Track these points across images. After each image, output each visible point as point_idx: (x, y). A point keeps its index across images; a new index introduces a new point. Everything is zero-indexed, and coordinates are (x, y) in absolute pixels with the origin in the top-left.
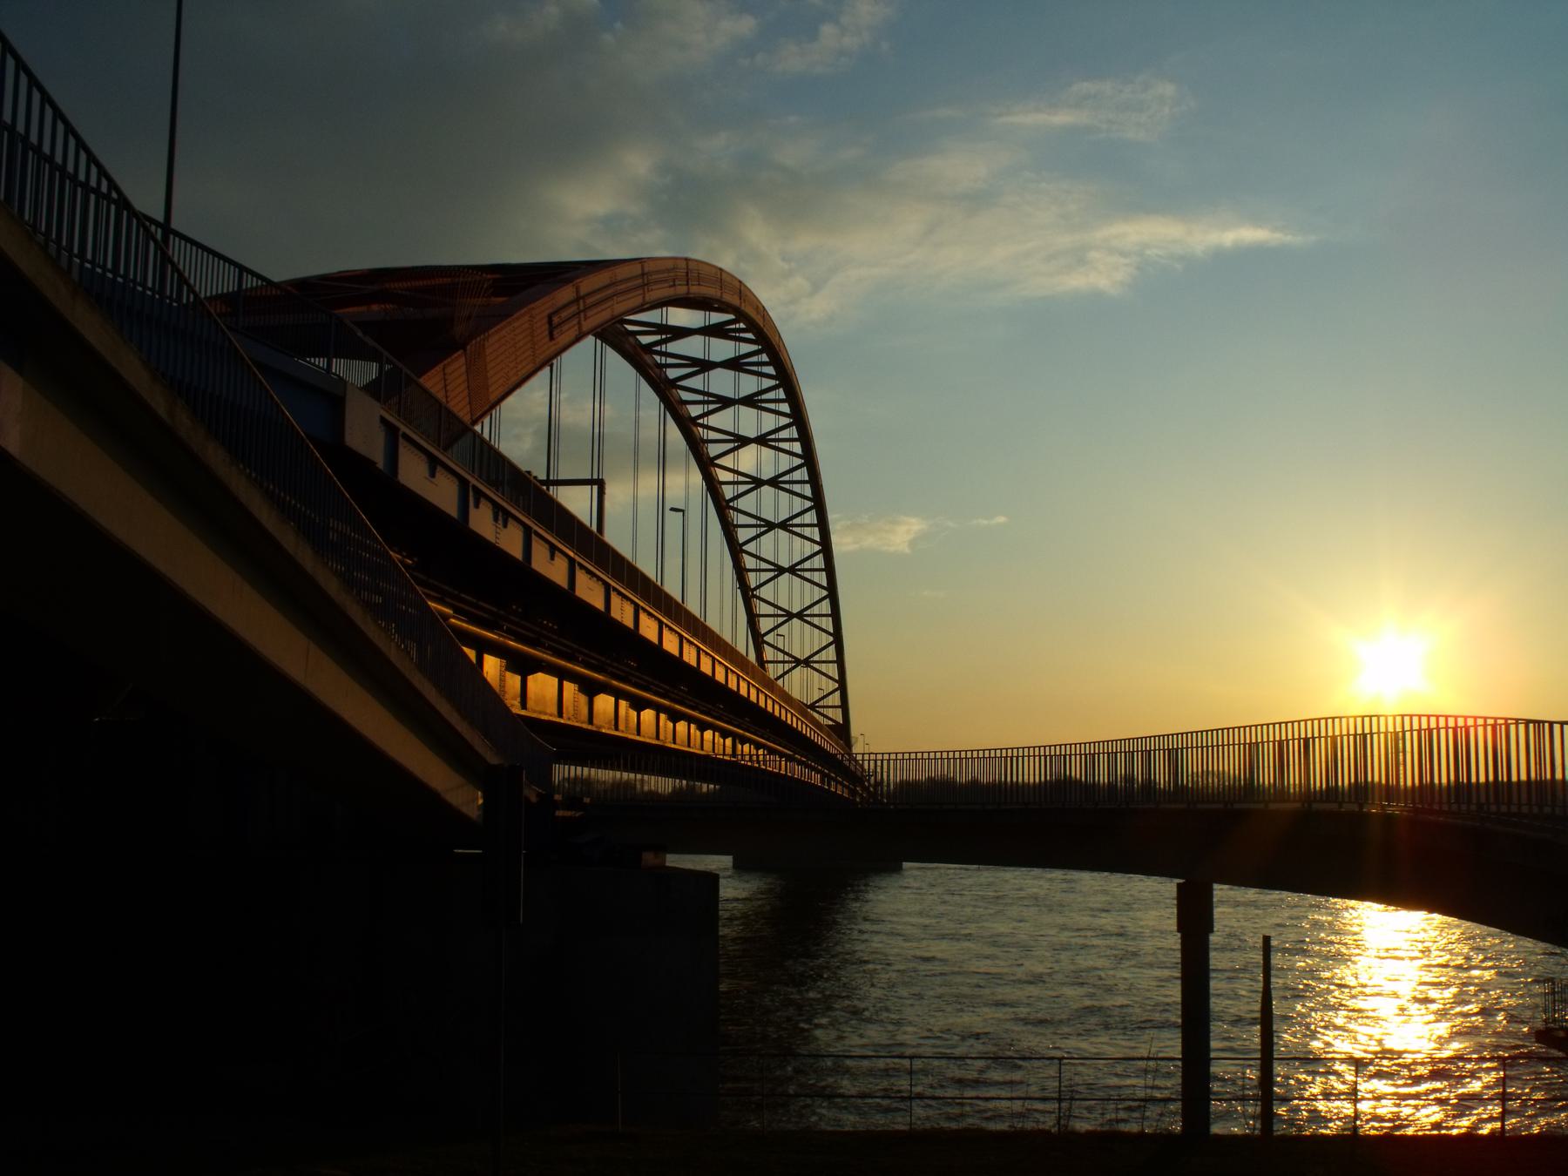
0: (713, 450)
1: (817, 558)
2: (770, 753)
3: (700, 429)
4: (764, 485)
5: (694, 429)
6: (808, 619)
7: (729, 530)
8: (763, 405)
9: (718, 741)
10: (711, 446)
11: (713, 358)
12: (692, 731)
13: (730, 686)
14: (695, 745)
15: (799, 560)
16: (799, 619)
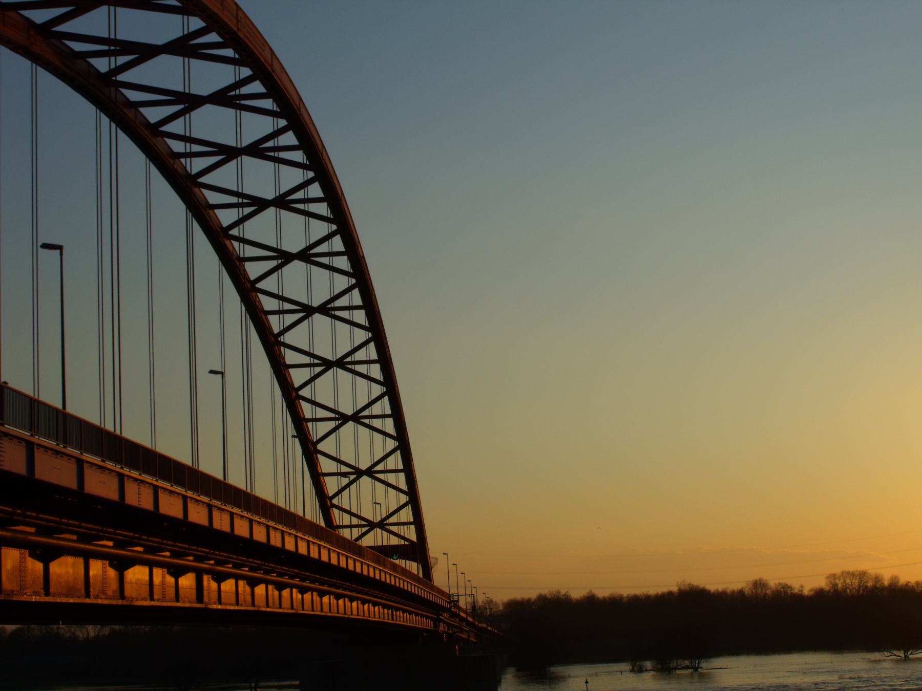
0: (226, 217)
1: (404, 511)
2: (374, 606)
3: (236, 244)
4: (314, 313)
5: (227, 242)
6: (366, 421)
7: (280, 369)
8: (243, 102)
9: (333, 603)
10: (219, 212)
11: (178, 60)
12: (314, 598)
13: (341, 565)
14: (317, 608)
15: (348, 349)
16: (355, 421)
